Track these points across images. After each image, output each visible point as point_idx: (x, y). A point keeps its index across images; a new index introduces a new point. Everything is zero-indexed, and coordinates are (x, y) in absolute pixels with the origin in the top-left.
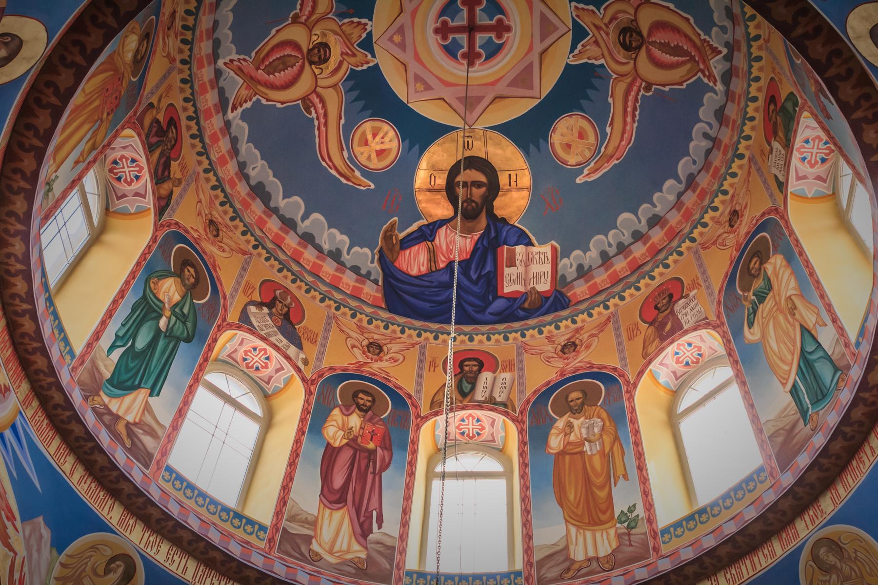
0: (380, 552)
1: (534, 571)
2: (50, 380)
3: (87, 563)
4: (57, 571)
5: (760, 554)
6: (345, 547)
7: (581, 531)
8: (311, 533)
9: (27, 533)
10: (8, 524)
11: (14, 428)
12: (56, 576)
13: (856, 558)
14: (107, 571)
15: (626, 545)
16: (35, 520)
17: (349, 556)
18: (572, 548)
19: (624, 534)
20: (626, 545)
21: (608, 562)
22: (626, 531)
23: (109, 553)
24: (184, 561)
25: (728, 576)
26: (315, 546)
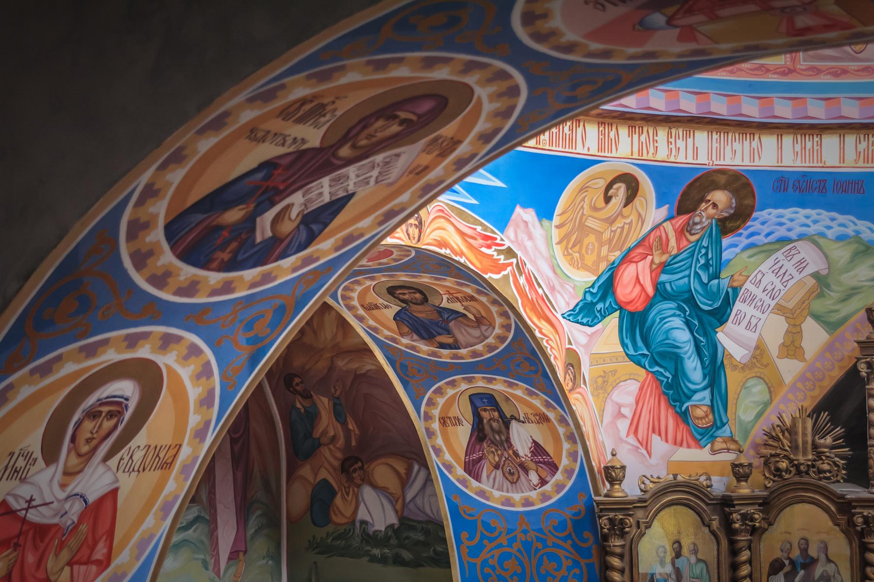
3: (582, 207)
4: (555, 240)
12: (558, 240)
14: (607, 199)
23: (602, 184)
24: (690, 141)
25: (798, 148)
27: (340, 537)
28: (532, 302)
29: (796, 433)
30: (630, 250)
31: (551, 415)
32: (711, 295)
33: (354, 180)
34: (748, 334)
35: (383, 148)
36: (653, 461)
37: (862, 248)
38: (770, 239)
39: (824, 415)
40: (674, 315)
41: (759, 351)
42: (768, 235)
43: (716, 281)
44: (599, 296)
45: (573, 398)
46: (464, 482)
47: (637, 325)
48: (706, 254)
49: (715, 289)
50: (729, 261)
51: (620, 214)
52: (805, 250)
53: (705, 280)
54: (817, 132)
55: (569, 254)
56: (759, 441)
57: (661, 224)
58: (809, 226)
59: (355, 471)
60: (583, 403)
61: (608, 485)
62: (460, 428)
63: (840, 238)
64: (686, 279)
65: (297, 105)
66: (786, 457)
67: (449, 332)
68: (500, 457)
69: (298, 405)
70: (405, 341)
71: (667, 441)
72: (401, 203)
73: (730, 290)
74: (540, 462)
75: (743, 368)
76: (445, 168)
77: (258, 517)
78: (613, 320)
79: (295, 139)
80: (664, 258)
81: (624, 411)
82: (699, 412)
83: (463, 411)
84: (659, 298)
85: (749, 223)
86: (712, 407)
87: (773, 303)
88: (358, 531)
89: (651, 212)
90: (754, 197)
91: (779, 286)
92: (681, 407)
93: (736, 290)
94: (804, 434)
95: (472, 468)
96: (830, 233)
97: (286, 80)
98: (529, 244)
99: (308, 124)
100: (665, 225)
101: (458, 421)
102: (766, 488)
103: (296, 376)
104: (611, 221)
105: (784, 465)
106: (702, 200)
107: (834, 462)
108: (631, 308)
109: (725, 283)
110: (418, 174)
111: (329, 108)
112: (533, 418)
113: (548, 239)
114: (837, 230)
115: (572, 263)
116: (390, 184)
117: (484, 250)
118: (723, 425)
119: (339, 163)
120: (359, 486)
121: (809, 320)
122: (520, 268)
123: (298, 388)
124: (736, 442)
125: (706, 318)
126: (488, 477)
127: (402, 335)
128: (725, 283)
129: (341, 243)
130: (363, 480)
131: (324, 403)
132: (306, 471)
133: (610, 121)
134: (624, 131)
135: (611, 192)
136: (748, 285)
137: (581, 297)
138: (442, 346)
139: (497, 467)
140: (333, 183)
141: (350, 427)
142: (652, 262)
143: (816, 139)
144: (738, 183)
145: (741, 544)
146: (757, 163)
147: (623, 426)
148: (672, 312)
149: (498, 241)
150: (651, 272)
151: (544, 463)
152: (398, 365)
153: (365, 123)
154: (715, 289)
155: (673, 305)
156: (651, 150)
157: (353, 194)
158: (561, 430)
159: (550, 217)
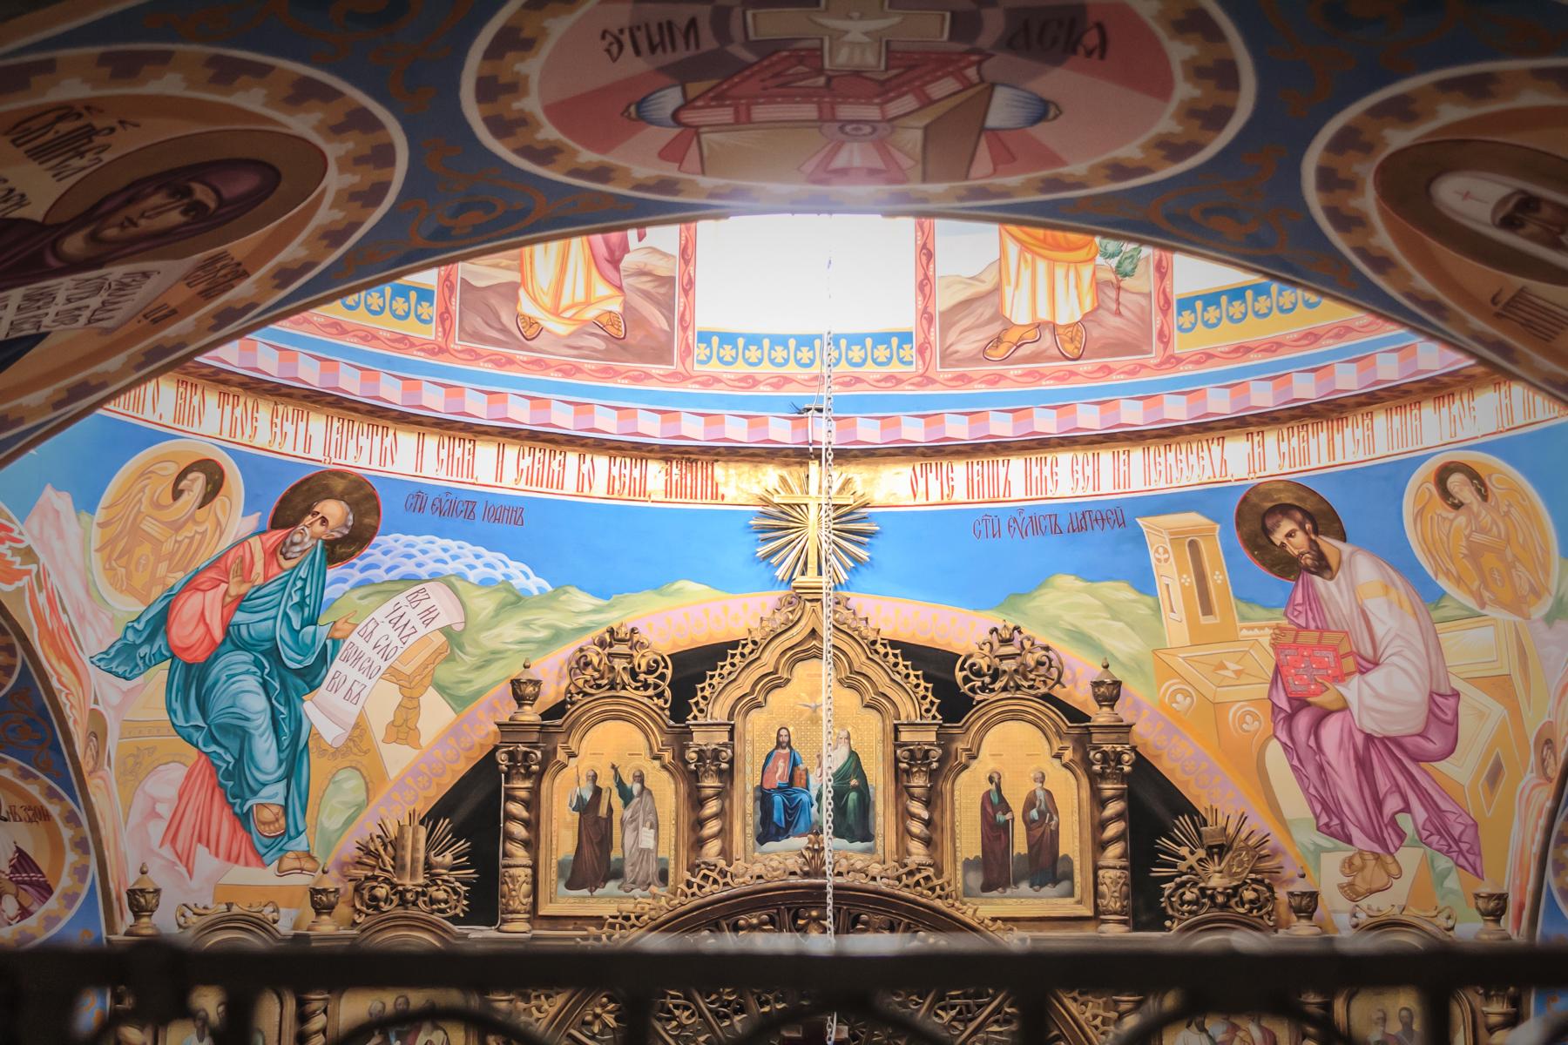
0: (647, 295)
1: (935, 336)
3: (140, 501)
4: (95, 544)
5: (1348, 431)
6: (580, 296)
7: (1029, 257)
8: (513, 276)
13: (1507, 514)
14: (177, 494)
15: (1108, 310)
16: (41, 501)
17: (590, 314)
18: (1008, 291)
19: (1108, 283)
20: (1108, 310)
21: (1072, 340)
22: (1111, 277)
23: (173, 470)
24: (302, 426)
26: (526, 307)
28: (52, 634)
29: (403, 848)
30: (198, 573)
31: (54, 810)
32: (303, 650)
33: (60, 308)
35: (132, 254)
36: (195, 884)
37: (513, 598)
38: (394, 575)
39: (444, 824)
40: (247, 672)
41: (360, 729)
42: (388, 571)
43: (311, 629)
44: (145, 635)
45: (93, 784)
47: (193, 680)
48: (303, 589)
49: (308, 641)
51: (192, 518)
52: (438, 596)
53: (297, 627)
54: (471, 436)
56: (346, 857)
57: (246, 539)
58: (445, 562)
60: (104, 791)
61: (129, 918)
63: (485, 583)
64: (270, 622)
65: (51, 117)
66: (386, 881)
71: (217, 855)
72: (107, 372)
73: (329, 643)
74: (24, 882)
75: (334, 754)
76: (199, 320)
78: (160, 672)
79: (11, 190)
80: (244, 588)
82: (267, 815)
84: (229, 646)
85: (367, 551)
86: (285, 808)
87: (385, 665)
89: (237, 520)
90: (379, 514)
91: (396, 642)
92: (241, 806)
94: (415, 849)
96: (472, 576)
97: (61, 54)
98: (57, 545)
99: (45, 166)
102: (354, 924)
104: (177, 527)
105: (382, 892)
106: (308, 510)
107: (453, 889)
108: (188, 657)
109: (323, 631)
110: (155, 321)
111: (98, 140)
112: (22, 813)
114: (481, 571)
116: (107, 331)
118: (299, 834)
119: (52, 262)
122: (41, 579)
124: (313, 858)
125: (292, 680)
128: (323, 631)
129: (64, 395)
133: (195, 380)
134: (212, 399)
135: (182, 485)
136: (354, 637)
137: (120, 634)
140: (26, 304)
142: (226, 592)
143: (1256, 439)
145: (314, 1006)
146: (389, 467)
147: (157, 830)
148: (245, 668)
149: (15, 535)
150: (223, 607)
151: (31, 884)
153: (134, 192)
154: (308, 641)
155: (246, 657)
156: (248, 431)
157: (46, 334)
158: (67, 833)
159: (91, 507)
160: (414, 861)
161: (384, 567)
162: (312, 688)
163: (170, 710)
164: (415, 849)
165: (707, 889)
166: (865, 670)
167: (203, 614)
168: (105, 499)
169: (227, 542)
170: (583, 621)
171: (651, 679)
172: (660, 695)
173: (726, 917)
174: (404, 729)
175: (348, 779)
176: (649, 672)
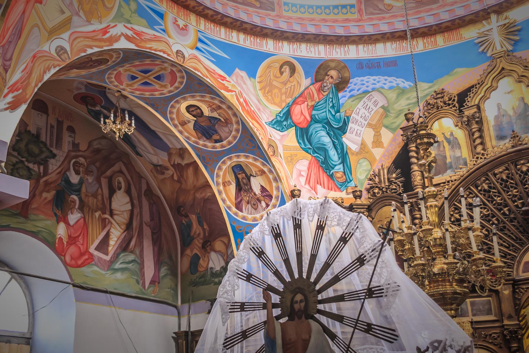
2: (201, 8)
3: (270, 75)
4: (258, 88)
9: (235, 80)
10: (224, 82)
11: (200, 40)
14: (282, 73)
16: (235, 72)
23: (278, 65)
24: (316, 48)
27: (203, 276)
31: (265, 170)
32: (338, 121)
34: (357, 138)
37: (401, 91)
40: (321, 130)
41: (363, 145)
42: (358, 90)
43: (339, 114)
45: (273, 159)
46: (236, 214)
47: (304, 134)
48: (332, 101)
49: (339, 118)
50: (343, 104)
51: (289, 80)
52: (376, 96)
53: (334, 114)
55: (266, 96)
59: (208, 246)
62: (231, 186)
63: (391, 88)
66: (377, 187)
67: (216, 132)
68: (249, 197)
69: (184, 222)
70: (201, 142)
71: (324, 188)
73: (346, 118)
77: (165, 269)
80: (313, 103)
81: (302, 173)
82: (339, 175)
83: (231, 178)
84: (313, 122)
85: (349, 85)
86: (344, 172)
87: (366, 123)
88: (209, 273)
89: (304, 82)
91: (368, 114)
93: (348, 117)
94: (384, 175)
95: (238, 206)
96: (386, 87)
98: (244, 86)
100: (311, 87)
101: (230, 183)
103: (182, 207)
104: (285, 83)
112: (258, 173)
113: (255, 87)
115: (268, 100)
117: (219, 80)
118: (351, 181)
120: (209, 253)
121: (383, 128)
123: (183, 213)
125: (336, 131)
126: (245, 209)
127: (199, 139)
128: (343, 114)
130: (211, 250)
131: (193, 218)
132: (188, 252)
135: (283, 70)
136: (353, 115)
138: (216, 141)
139: (248, 203)
141: (205, 227)
142: (308, 105)
144: (341, 66)
146: (348, 56)
148: (320, 129)
151: (267, 196)
152: (201, 158)
155: (320, 125)
158: (271, 177)
160: (384, 178)
161: (356, 90)
162: (344, 133)
163: (299, 143)
164: (384, 175)
165: (478, 162)
166: (524, 74)
167: (302, 112)
168: (258, 74)
169: (303, 88)
170: (426, 92)
171: (450, 102)
172: (454, 106)
173: (490, 170)
174: (378, 143)
175: (363, 162)
176: (449, 100)
